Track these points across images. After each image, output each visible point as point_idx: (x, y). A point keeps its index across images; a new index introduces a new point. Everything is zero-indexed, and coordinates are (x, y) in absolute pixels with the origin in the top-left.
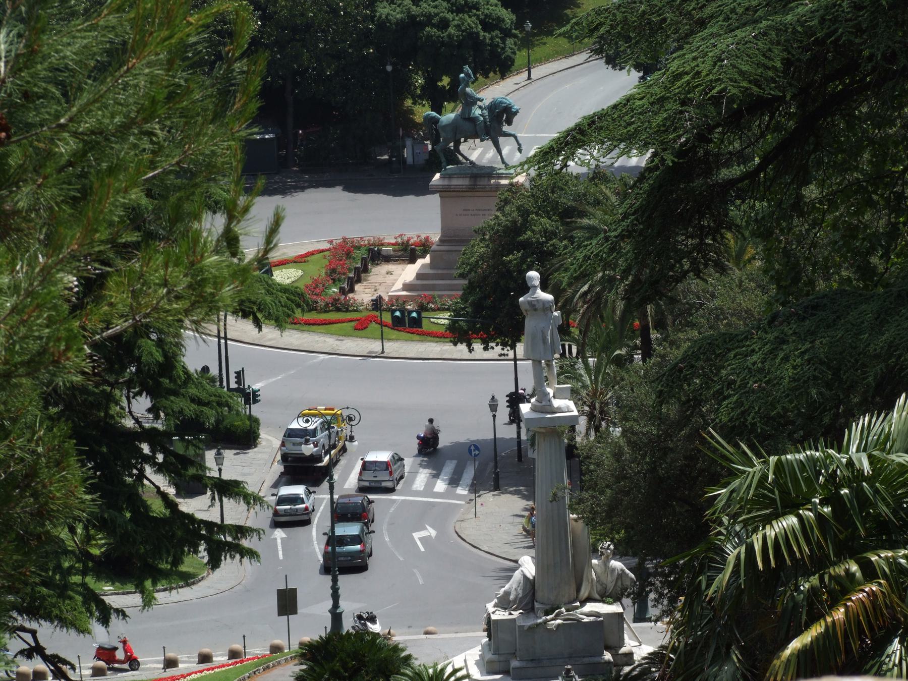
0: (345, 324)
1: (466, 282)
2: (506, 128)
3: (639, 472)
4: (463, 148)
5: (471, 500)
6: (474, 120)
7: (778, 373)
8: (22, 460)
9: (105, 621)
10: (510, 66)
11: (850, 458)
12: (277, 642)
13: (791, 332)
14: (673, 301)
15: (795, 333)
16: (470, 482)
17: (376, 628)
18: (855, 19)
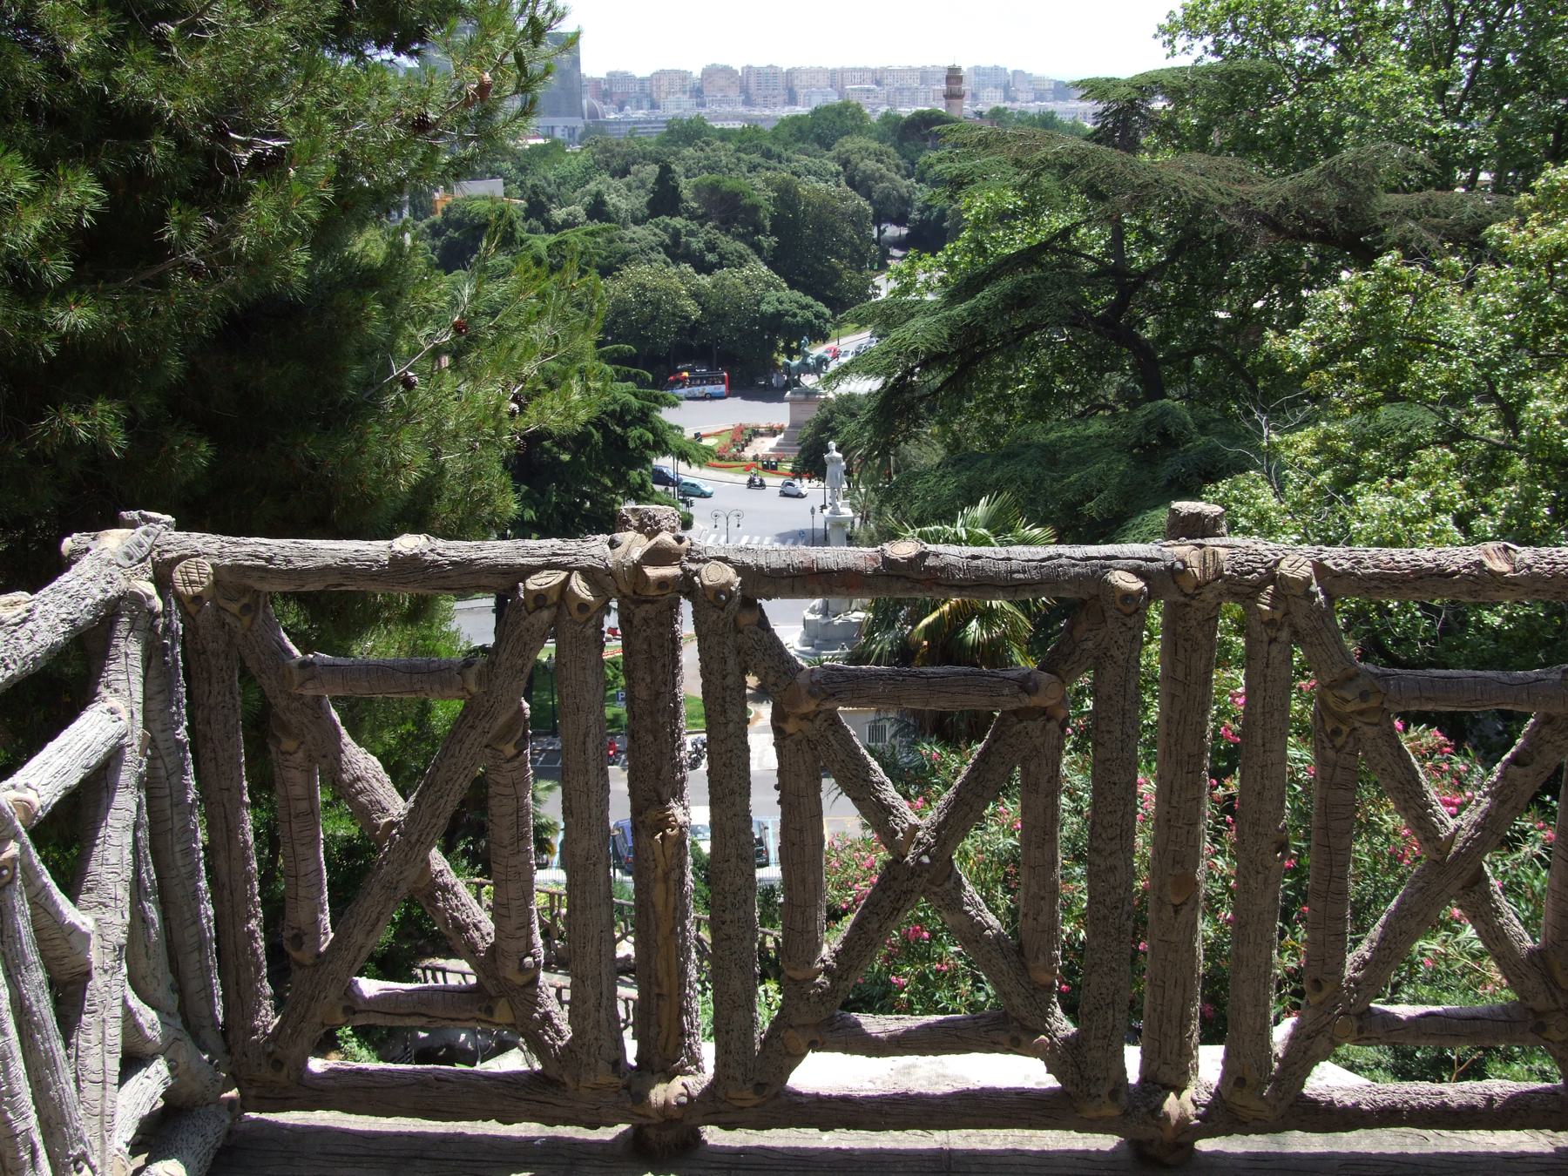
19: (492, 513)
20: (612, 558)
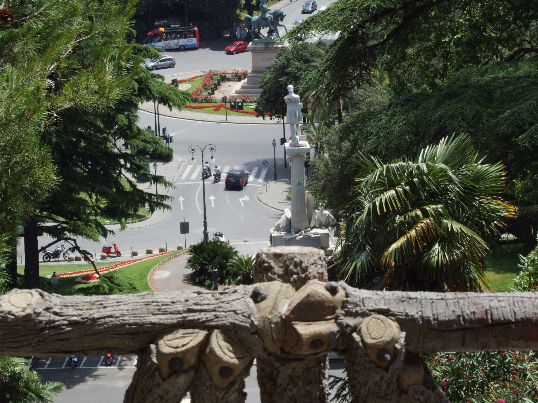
2: (280, 23)
3: (336, 173)
6: (266, 19)
8: (28, 161)
9: (105, 235)
12: (180, 245)
14: (351, 99)
15: (399, 112)
17: (222, 239)
19: (34, 184)
20: (258, 314)
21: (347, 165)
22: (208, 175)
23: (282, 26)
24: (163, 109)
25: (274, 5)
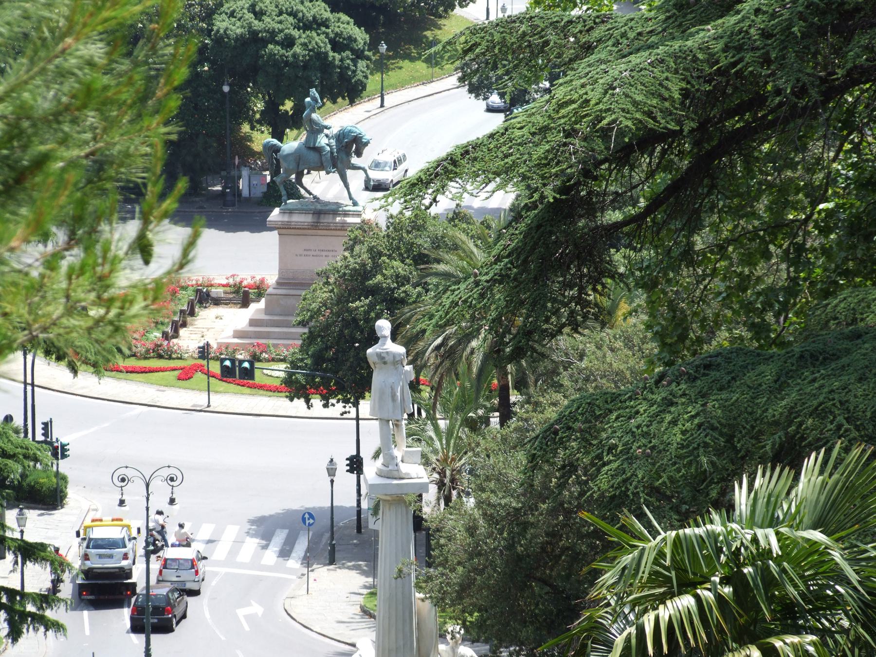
0: (168, 373)
1: (306, 330)
2: (355, 160)
3: (495, 549)
4: (306, 180)
5: (303, 575)
6: (318, 150)
7: (665, 437)
10: (361, 91)
11: (755, 534)
13: (680, 392)
15: (684, 395)
16: (302, 554)
18: (763, 48)
21: (525, 530)
22: (159, 544)
23: (359, 168)
24: (50, 372)
25: (339, 115)
